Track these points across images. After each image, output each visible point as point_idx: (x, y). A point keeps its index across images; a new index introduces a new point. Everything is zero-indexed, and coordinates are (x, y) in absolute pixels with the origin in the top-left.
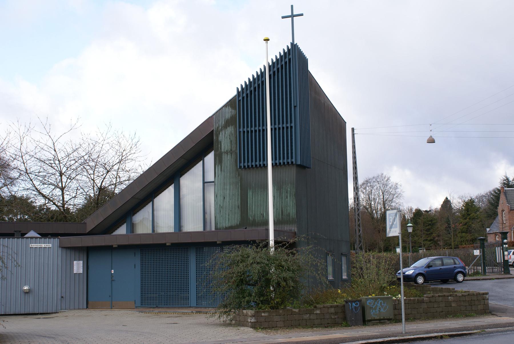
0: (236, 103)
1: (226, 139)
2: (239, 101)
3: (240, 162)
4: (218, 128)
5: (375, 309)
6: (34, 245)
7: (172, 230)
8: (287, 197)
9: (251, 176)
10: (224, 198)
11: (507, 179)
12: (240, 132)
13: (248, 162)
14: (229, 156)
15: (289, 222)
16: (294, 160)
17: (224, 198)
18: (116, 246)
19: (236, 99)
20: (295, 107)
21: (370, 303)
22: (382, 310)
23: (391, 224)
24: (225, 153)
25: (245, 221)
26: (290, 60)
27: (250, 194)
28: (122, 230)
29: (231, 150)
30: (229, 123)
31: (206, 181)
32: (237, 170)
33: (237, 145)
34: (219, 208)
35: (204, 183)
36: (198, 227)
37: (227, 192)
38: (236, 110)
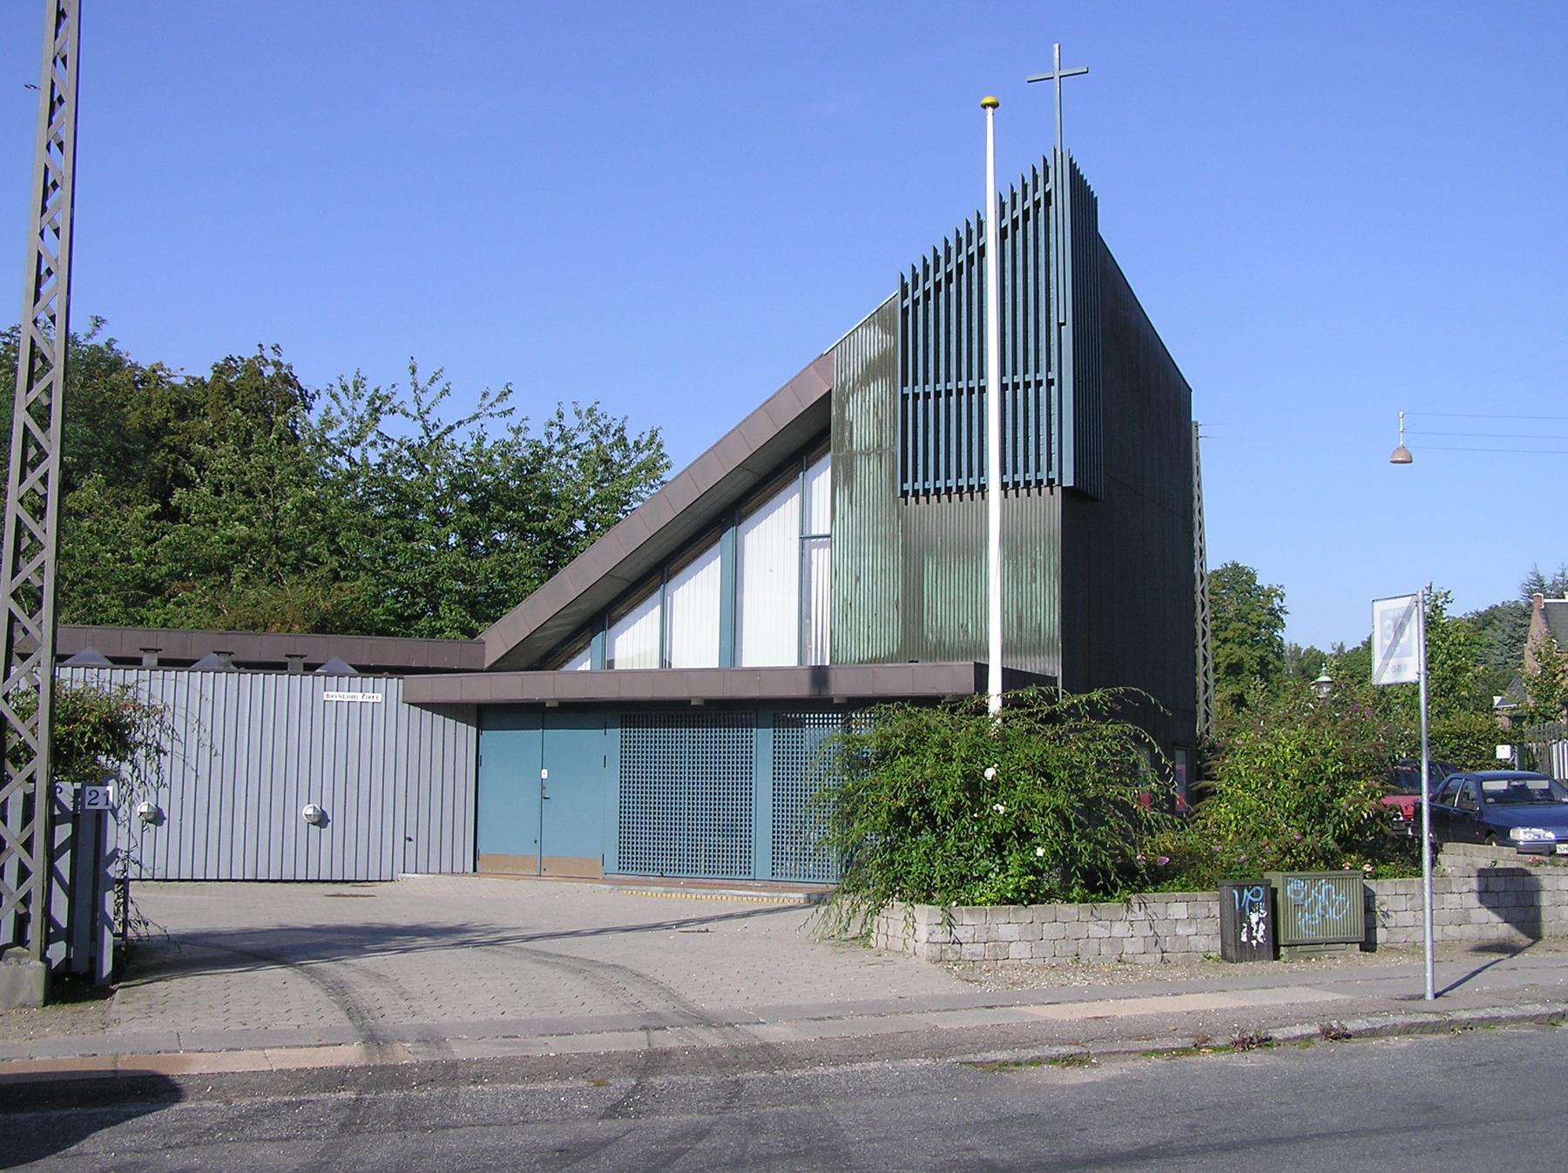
0: (895, 316)
1: (865, 419)
2: (905, 311)
3: (904, 480)
4: (843, 385)
5: (1311, 910)
6: (333, 696)
7: (712, 662)
8: (1034, 579)
9: (936, 515)
10: (858, 579)
11: (1540, 579)
12: (905, 397)
13: (930, 459)
14: (874, 463)
15: (1036, 649)
16: (1054, 474)
17: (858, 579)
18: (555, 704)
19: (895, 304)
20: (1060, 325)
21: (1296, 893)
22: (1332, 914)
23: (1388, 642)
24: (862, 453)
25: (914, 647)
26: (1048, 195)
27: (930, 567)
28: (583, 663)
29: (880, 446)
30: (872, 371)
31: (807, 534)
32: (895, 500)
33: (895, 431)
34: (844, 608)
35: (802, 539)
36: (787, 658)
37: (868, 561)
38: (895, 334)
